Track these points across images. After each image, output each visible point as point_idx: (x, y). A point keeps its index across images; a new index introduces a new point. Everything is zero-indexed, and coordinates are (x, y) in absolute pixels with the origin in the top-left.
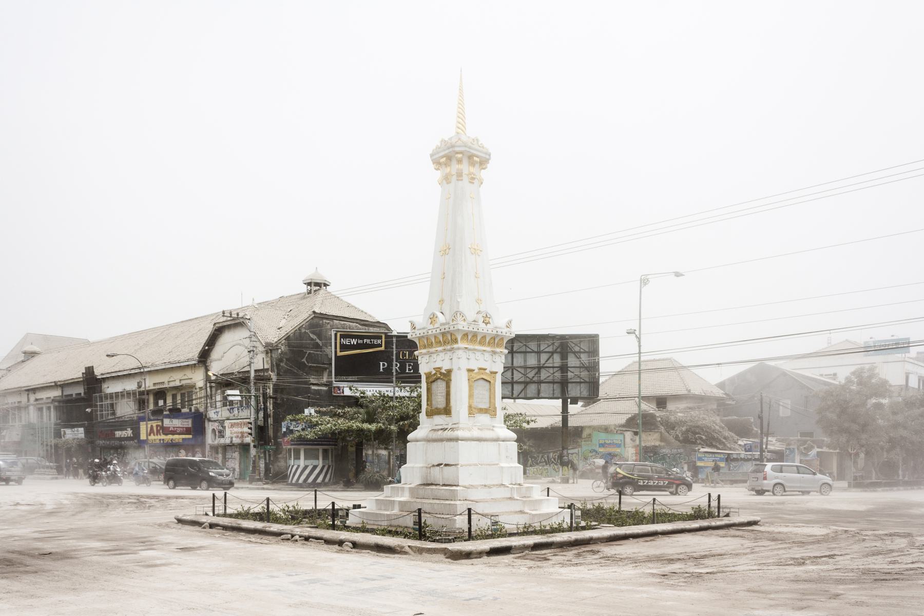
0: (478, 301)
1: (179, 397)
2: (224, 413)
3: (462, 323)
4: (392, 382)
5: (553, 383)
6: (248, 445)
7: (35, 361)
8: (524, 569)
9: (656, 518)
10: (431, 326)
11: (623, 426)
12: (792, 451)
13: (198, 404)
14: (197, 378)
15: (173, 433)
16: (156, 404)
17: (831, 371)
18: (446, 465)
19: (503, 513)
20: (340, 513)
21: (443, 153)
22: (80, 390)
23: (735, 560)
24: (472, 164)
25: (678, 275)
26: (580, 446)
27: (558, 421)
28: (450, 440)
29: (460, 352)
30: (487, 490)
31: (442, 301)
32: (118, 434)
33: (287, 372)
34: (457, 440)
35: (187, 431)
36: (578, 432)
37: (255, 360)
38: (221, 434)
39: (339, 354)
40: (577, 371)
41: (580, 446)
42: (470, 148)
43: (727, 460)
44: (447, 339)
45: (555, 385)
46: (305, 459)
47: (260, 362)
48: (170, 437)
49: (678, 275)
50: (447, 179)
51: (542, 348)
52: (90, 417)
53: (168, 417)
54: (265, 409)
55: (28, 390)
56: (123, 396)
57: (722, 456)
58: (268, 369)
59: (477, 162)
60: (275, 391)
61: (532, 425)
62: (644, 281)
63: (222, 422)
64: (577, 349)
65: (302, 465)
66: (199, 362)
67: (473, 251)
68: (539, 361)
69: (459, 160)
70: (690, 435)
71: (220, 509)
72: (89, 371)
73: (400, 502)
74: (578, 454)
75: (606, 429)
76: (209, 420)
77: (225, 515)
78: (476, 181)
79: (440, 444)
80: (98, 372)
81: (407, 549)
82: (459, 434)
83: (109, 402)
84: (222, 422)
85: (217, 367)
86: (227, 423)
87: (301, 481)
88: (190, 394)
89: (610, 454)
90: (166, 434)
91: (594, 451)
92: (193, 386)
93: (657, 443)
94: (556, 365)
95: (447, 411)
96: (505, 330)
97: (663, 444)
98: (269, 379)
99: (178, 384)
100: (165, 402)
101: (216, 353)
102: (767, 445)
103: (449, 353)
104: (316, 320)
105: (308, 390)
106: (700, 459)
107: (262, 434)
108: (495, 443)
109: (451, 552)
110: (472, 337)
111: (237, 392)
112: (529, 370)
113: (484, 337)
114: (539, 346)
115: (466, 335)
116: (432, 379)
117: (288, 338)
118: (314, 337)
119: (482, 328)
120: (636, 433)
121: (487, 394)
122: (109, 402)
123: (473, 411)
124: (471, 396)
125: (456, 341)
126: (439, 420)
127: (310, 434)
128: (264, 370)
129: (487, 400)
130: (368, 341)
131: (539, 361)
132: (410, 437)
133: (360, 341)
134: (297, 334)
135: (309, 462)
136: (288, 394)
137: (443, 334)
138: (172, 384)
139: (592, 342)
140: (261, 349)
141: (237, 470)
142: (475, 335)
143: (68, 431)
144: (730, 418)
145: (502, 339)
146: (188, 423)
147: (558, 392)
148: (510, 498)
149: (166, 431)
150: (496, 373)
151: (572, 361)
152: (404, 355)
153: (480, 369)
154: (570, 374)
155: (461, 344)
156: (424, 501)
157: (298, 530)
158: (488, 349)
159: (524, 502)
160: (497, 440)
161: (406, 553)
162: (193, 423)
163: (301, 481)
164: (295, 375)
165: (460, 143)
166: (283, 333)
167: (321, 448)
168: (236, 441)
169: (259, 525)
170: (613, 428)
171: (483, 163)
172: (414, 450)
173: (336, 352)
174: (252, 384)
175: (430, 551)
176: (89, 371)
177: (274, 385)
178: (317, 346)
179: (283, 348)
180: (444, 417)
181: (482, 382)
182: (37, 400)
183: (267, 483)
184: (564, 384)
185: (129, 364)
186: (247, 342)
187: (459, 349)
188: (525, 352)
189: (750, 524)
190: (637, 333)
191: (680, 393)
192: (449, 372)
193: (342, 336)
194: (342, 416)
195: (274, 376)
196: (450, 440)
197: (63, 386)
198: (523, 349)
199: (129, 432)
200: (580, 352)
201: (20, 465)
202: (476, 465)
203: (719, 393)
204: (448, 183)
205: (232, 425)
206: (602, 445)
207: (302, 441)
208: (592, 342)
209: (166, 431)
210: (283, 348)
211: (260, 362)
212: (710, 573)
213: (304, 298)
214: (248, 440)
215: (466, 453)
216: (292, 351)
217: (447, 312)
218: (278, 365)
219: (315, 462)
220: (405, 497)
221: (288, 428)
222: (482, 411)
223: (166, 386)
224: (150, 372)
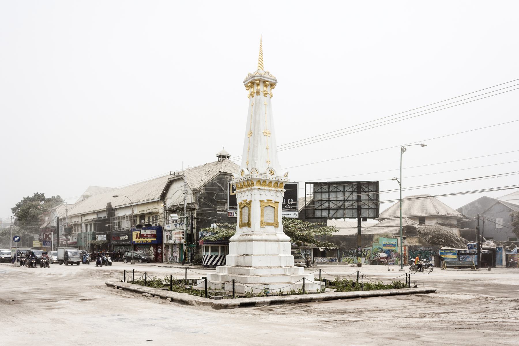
0: (268, 162)
1: (151, 218)
2: (172, 226)
3: (257, 174)
5: (353, 209)
6: (182, 244)
7: (88, 200)
8: (250, 315)
9: (355, 286)
10: (241, 177)
11: (397, 234)
12: (500, 249)
13: (160, 222)
14: (160, 208)
15: (147, 237)
16: (140, 222)
18: (247, 255)
19: (274, 284)
20: (190, 282)
21: (248, 81)
22: (104, 215)
23: (379, 314)
24: (266, 86)
25: (422, 145)
26: (372, 246)
27: (355, 232)
28: (249, 241)
29: (255, 191)
30: (269, 269)
31: (248, 163)
32: (122, 238)
33: (205, 204)
34: (252, 240)
35: (154, 236)
36: (370, 238)
37: (187, 198)
38: (169, 238)
39: (231, 194)
40: (367, 202)
41: (372, 246)
42: (263, 77)
43: (458, 254)
44: (249, 183)
45: (354, 211)
46: (212, 251)
47: (190, 199)
48: (146, 239)
49: (422, 145)
51: (346, 189)
53: (144, 229)
54: (192, 224)
55: (82, 215)
56: (124, 218)
57: (455, 252)
58: (193, 203)
59: (268, 85)
60: (197, 214)
61: (337, 234)
62: (403, 150)
63: (170, 232)
64: (366, 190)
65: (209, 256)
66: (161, 199)
67: (265, 134)
68: (344, 197)
69: (259, 84)
70: (435, 240)
71: (129, 278)
72: (109, 204)
73: (222, 276)
74: (371, 250)
75: (387, 236)
76: (165, 231)
77: (133, 282)
78: (268, 95)
79: (244, 243)
80: (113, 206)
81: (194, 303)
82: (254, 237)
83: (118, 221)
84: (170, 232)
85: (170, 202)
86: (173, 232)
87: (208, 264)
88: (156, 216)
89: (389, 250)
90: (144, 238)
91: (380, 248)
92: (158, 213)
93: (417, 244)
94: (354, 199)
95: (249, 224)
96: (283, 179)
97: (420, 244)
98: (195, 208)
99: (150, 211)
100: (144, 221)
101: (169, 195)
102: (482, 245)
103: (250, 192)
104: (221, 176)
105: (216, 214)
106: (442, 253)
107: (189, 238)
108: (276, 243)
109: (215, 305)
110: (263, 182)
111: (176, 215)
112: (338, 202)
113: (270, 182)
114: (344, 188)
115: (259, 181)
117: (205, 186)
118: (220, 185)
119: (269, 177)
121: (273, 215)
122: (118, 221)
124: (262, 216)
125: (253, 185)
126: (245, 229)
127: (213, 239)
129: (273, 218)
131: (344, 197)
132: (231, 239)
134: (211, 183)
135: (213, 254)
136: (205, 216)
137: (247, 181)
138: (148, 211)
139: (375, 185)
140: (190, 192)
141: (178, 258)
142: (265, 181)
143: (99, 236)
144: (465, 229)
145: (282, 183)
146: (154, 232)
147: (355, 214)
148: (284, 275)
149: (142, 236)
150: (278, 202)
151: (364, 196)
153: (268, 200)
154: (362, 204)
155: (256, 187)
156: (236, 276)
157: (152, 290)
158: (246, 189)
159: (291, 277)
160: (278, 241)
161: (193, 305)
162: (157, 232)
163: (208, 264)
164: (209, 206)
165: (257, 74)
166: (203, 183)
167: (220, 246)
168: (177, 242)
169: (394, 291)
170: (391, 235)
172: (232, 246)
174: (185, 211)
175: (204, 304)
176: (109, 204)
177: (197, 212)
178: (221, 190)
179: (202, 191)
180: (247, 227)
181: (269, 208)
182: (86, 220)
183: (191, 265)
184: (359, 209)
185: (125, 202)
186: (183, 188)
187: (254, 189)
188: (337, 192)
189: (428, 292)
191: (433, 214)
192: (250, 202)
194: (232, 228)
195: (197, 207)
196: (249, 241)
197: (97, 213)
198: (335, 190)
199: (126, 237)
200: (369, 191)
201: (79, 254)
202: (264, 255)
203: (458, 215)
204: (253, 97)
205: (176, 233)
206: (384, 245)
207: (208, 242)
208: (375, 185)
209: (142, 236)
210: (202, 191)
211: (190, 199)
212: (357, 321)
213: (217, 164)
214: (183, 241)
215: (257, 248)
216: (208, 193)
217: (250, 169)
218: (199, 201)
219: (216, 254)
220: (225, 273)
221: (202, 235)
222: (268, 224)
223: (145, 212)
224: (137, 205)
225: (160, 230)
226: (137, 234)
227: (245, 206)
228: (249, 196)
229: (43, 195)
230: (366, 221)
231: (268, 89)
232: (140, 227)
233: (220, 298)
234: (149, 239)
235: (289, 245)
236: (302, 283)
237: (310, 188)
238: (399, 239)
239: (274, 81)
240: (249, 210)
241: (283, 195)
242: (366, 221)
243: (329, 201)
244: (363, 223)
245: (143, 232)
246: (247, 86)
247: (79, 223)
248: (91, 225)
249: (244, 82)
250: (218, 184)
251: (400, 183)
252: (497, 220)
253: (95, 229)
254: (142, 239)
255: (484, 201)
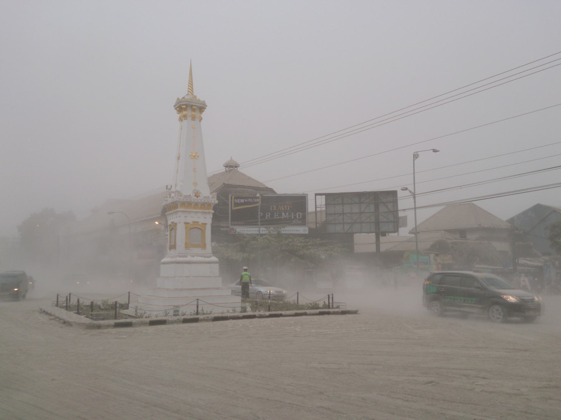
4: (258, 225)
24: (194, 110)
25: (435, 151)
39: (234, 208)
49: (435, 151)
50: (181, 120)
62: (416, 156)
69: (190, 108)
119: (194, 199)
120: (437, 255)
130: (251, 200)
133: (246, 200)
152: (273, 208)
171: (202, 108)
173: (231, 207)
184: (377, 223)
193: (235, 198)
208: (394, 193)
230: (385, 235)
231: (197, 114)
233: (100, 319)
236: (196, 303)
237: (322, 201)
238: (432, 256)
239: (202, 106)
240: (175, 233)
241: (211, 216)
242: (385, 235)
243: (343, 214)
244: (382, 239)
249: (174, 106)
255: (538, 209)
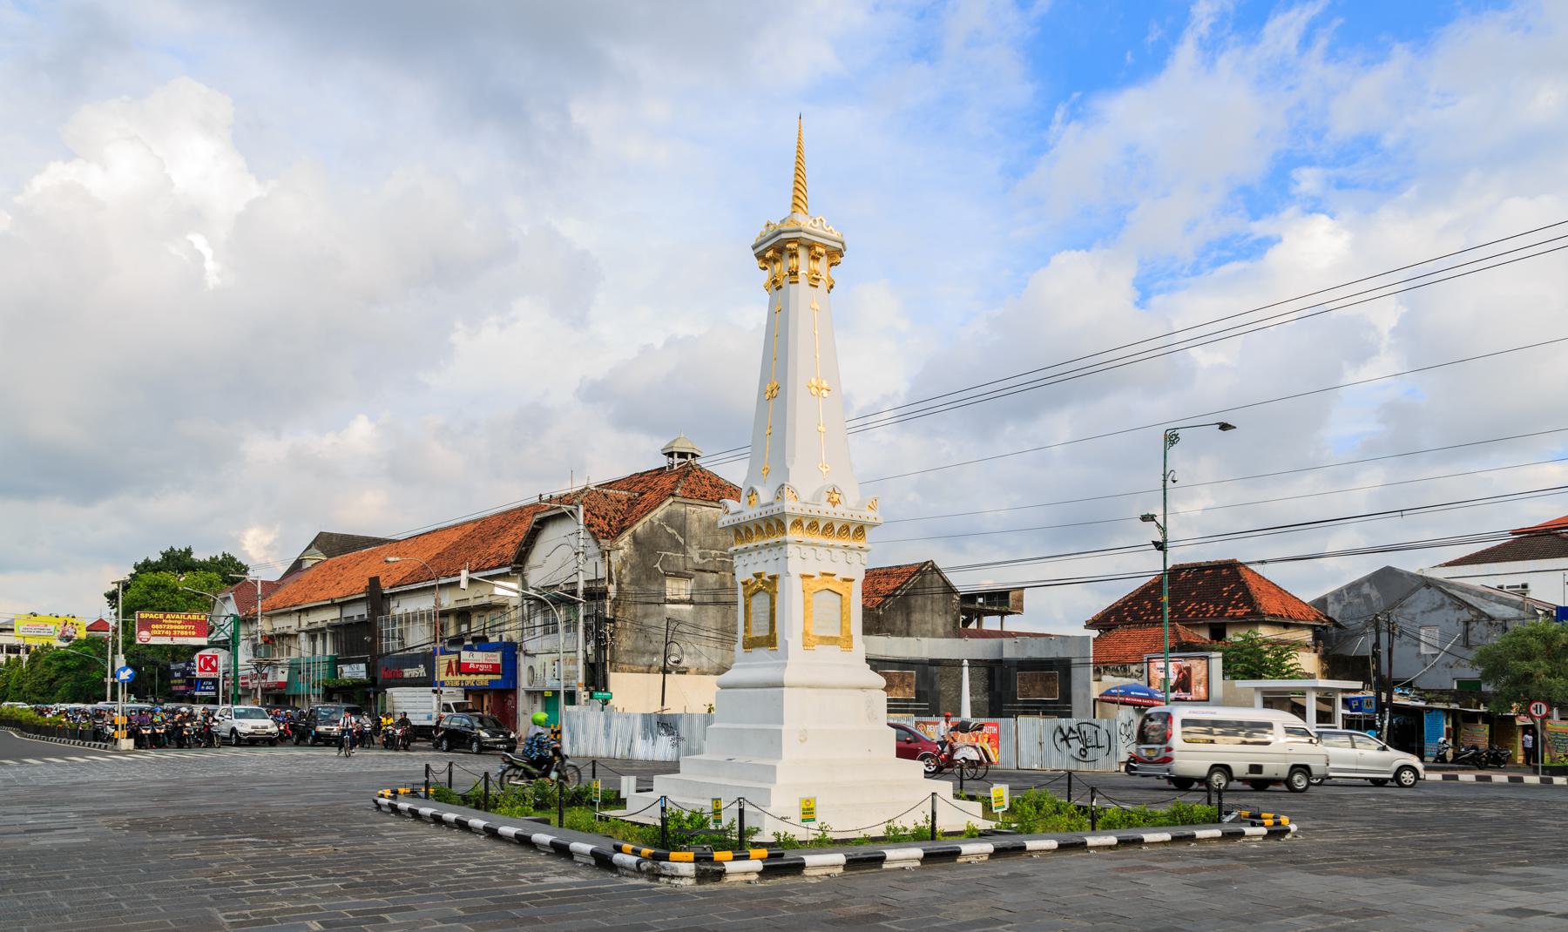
15: (477, 672)
17: (1518, 581)
22: (359, 612)
25: (1224, 427)
35: (495, 669)
48: (473, 677)
49: (1224, 427)
50: (775, 284)
52: (372, 647)
56: (415, 619)
62: (1171, 439)
90: (468, 674)
95: (770, 641)
101: (536, 557)
103: (775, 550)
116: (752, 591)
123: (808, 641)
128: (596, 581)
138: (478, 602)
143: (346, 668)
158: (762, 543)
176: (374, 581)
190: (1160, 519)
192: (774, 578)
223: (472, 603)
225: (511, 651)
226: (450, 663)
227: (759, 590)
228: (771, 562)
229: (188, 552)
232: (457, 641)
234: (481, 677)
235: (882, 698)
239: (839, 246)
245: (466, 656)
246: (760, 256)
247: (291, 631)
248: (324, 636)
249: (754, 248)
250: (669, 530)
251: (1164, 530)
252: (1423, 631)
253: (335, 648)
254: (464, 677)
255: (1386, 577)
